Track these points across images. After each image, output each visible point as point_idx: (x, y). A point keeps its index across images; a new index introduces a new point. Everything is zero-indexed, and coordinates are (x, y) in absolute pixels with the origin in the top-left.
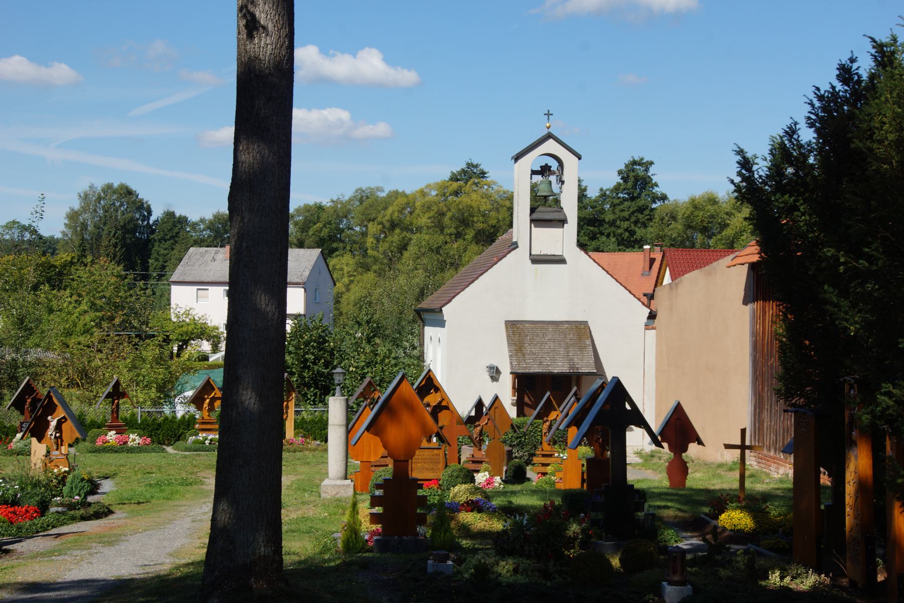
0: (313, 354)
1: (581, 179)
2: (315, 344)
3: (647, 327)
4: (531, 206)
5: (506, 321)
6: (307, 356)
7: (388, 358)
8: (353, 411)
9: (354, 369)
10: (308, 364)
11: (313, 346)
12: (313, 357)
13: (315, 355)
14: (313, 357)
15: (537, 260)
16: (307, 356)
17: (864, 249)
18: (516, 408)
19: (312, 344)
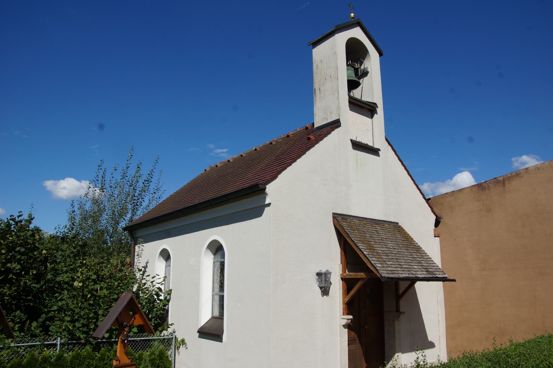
0: (19, 261)
1: (149, 262)
2: (23, 250)
3: (171, 290)
4: (347, 74)
5: (333, 213)
6: (9, 265)
7: (121, 281)
8: (80, 344)
9: (53, 247)
10: (11, 275)
11: (19, 252)
12: (19, 267)
13: (21, 265)
14: (19, 267)
15: (357, 146)
16: (9, 265)
17: (19, 320)
18: (347, 330)
19: (18, 248)
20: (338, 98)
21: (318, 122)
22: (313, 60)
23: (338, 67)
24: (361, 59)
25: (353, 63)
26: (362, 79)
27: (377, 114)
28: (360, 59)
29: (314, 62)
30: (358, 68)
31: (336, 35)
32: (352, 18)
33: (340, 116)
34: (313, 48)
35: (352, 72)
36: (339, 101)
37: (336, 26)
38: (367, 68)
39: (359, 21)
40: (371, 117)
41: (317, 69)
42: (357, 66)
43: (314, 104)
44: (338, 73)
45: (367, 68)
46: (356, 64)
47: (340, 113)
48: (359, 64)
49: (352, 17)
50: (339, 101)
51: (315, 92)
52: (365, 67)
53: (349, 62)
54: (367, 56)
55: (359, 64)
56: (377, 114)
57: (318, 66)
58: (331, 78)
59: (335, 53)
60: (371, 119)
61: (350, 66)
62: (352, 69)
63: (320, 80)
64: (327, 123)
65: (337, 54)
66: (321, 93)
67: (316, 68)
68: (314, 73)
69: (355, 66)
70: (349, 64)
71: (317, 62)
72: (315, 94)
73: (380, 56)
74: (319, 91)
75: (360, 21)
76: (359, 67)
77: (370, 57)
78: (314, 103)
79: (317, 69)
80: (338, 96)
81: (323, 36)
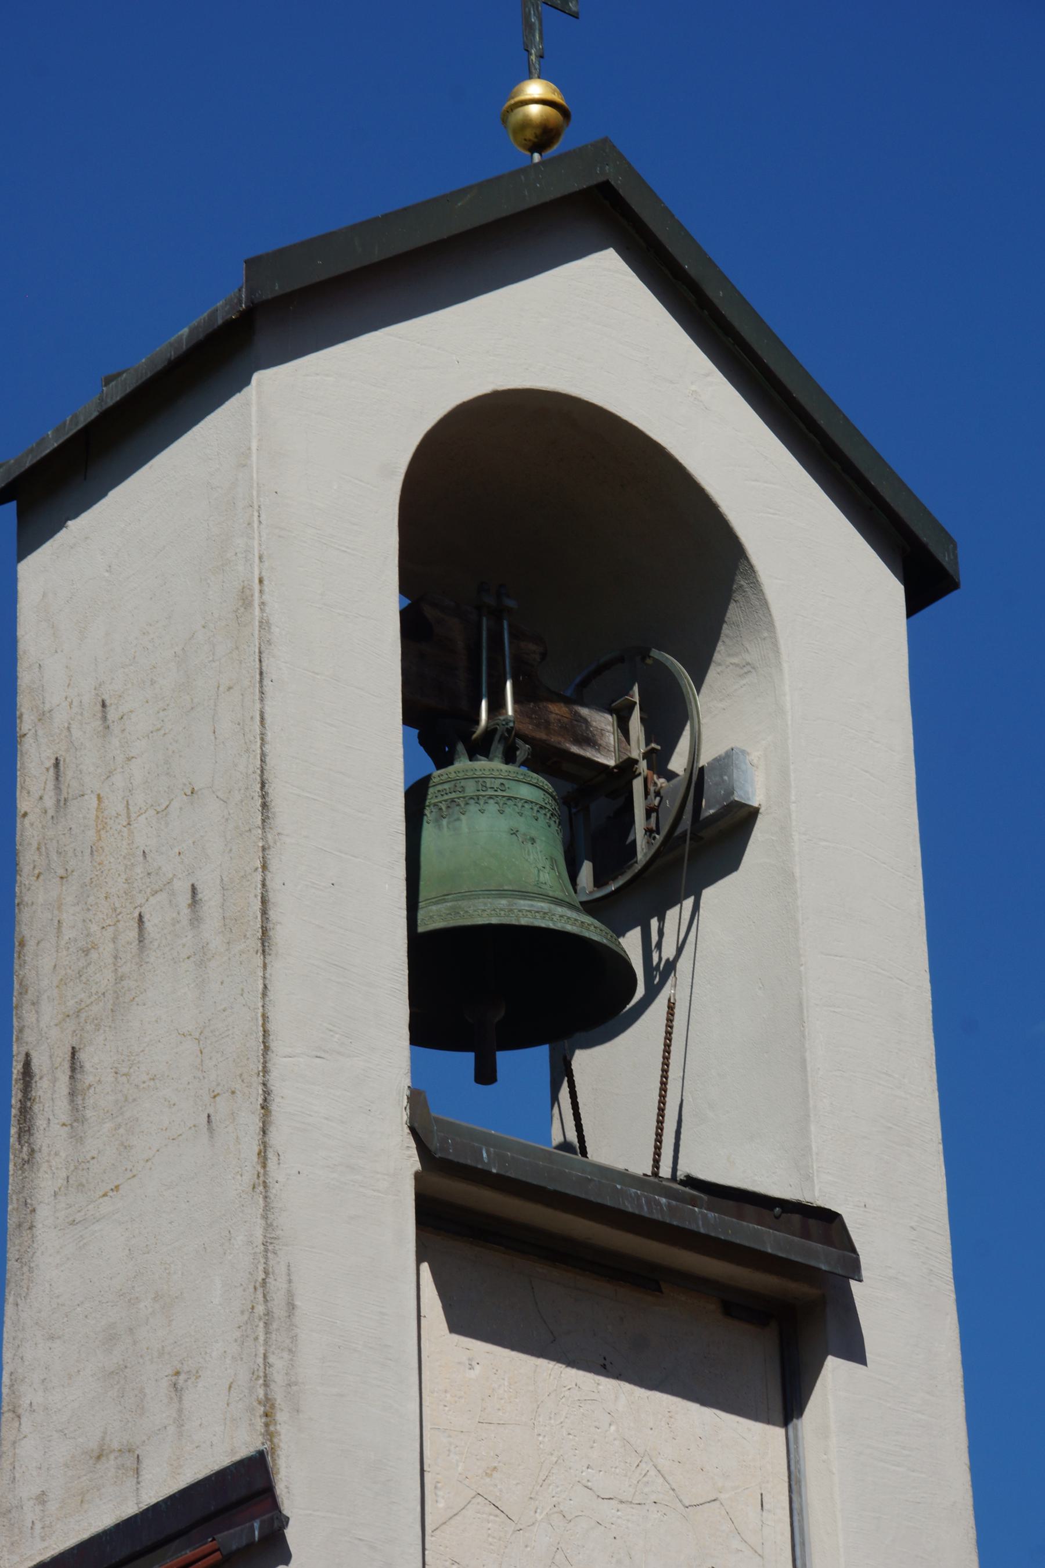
20: (263, 1185)
21: (42, 1499)
22: (25, 704)
23: (275, 791)
24: (655, 653)
25: (557, 711)
26: (679, 905)
27: (855, 1352)
28: (645, 654)
29: (27, 722)
30: (628, 767)
31: (257, 377)
32: (529, 134)
33: (281, 1416)
34: (27, 544)
35: (522, 824)
36: (269, 1226)
37: (251, 263)
38: (725, 762)
39: (608, 172)
40: (779, 1415)
41: (62, 804)
42: (611, 738)
43: (12, 1265)
44: (274, 864)
45: (725, 762)
46: (603, 722)
47: (278, 1378)
48: (636, 714)
49: (526, 124)
50: (269, 1226)
51: (25, 1111)
52: (704, 760)
53: (497, 705)
54: (734, 612)
55: (636, 714)
56: (855, 1352)
57: (69, 774)
58: (196, 920)
59: (246, 601)
60: (781, 1431)
61: (498, 748)
62: (525, 792)
63: (86, 952)
64: (130, 1509)
65: (265, 625)
66: (89, 1113)
67: (49, 802)
68: (28, 859)
69: (589, 741)
70: (490, 733)
71: (60, 718)
72: (26, 1130)
73: (914, 606)
74: (72, 1094)
75: (618, 182)
76: (637, 748)
77: (771, 625)
78: (12, 1253)
79: (62, 804)
80: (263, 1156)
81: (114, 394)
